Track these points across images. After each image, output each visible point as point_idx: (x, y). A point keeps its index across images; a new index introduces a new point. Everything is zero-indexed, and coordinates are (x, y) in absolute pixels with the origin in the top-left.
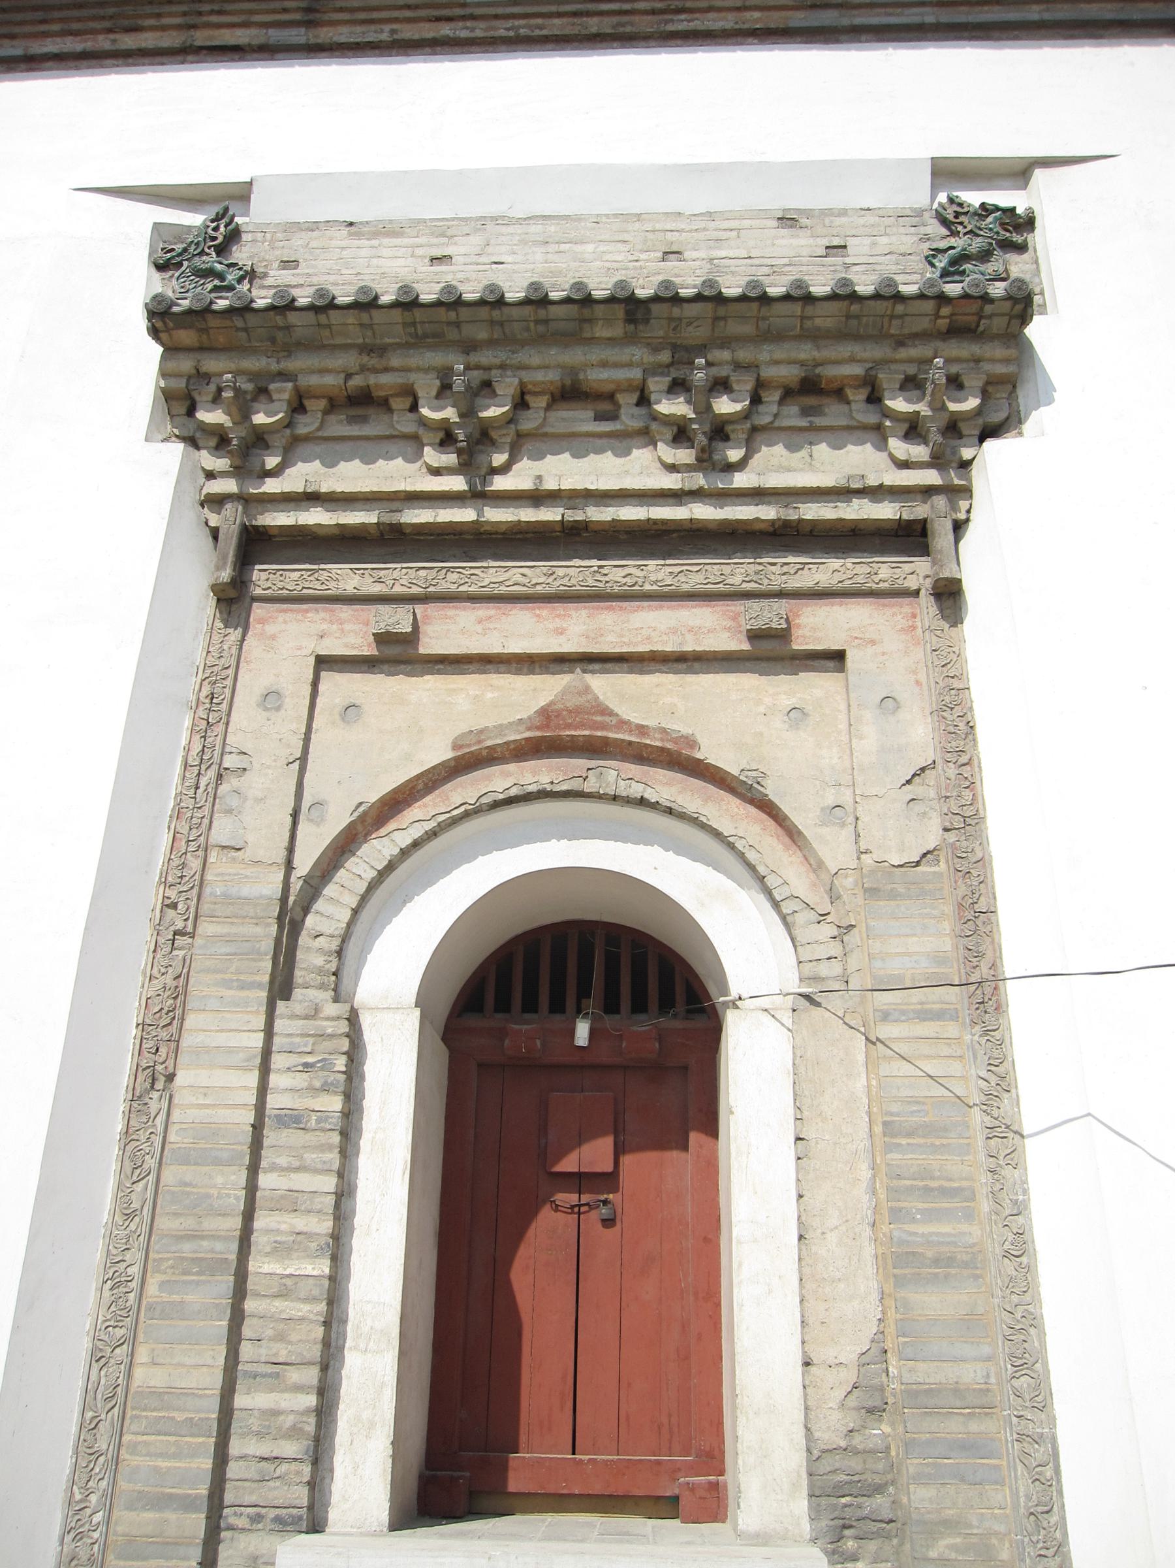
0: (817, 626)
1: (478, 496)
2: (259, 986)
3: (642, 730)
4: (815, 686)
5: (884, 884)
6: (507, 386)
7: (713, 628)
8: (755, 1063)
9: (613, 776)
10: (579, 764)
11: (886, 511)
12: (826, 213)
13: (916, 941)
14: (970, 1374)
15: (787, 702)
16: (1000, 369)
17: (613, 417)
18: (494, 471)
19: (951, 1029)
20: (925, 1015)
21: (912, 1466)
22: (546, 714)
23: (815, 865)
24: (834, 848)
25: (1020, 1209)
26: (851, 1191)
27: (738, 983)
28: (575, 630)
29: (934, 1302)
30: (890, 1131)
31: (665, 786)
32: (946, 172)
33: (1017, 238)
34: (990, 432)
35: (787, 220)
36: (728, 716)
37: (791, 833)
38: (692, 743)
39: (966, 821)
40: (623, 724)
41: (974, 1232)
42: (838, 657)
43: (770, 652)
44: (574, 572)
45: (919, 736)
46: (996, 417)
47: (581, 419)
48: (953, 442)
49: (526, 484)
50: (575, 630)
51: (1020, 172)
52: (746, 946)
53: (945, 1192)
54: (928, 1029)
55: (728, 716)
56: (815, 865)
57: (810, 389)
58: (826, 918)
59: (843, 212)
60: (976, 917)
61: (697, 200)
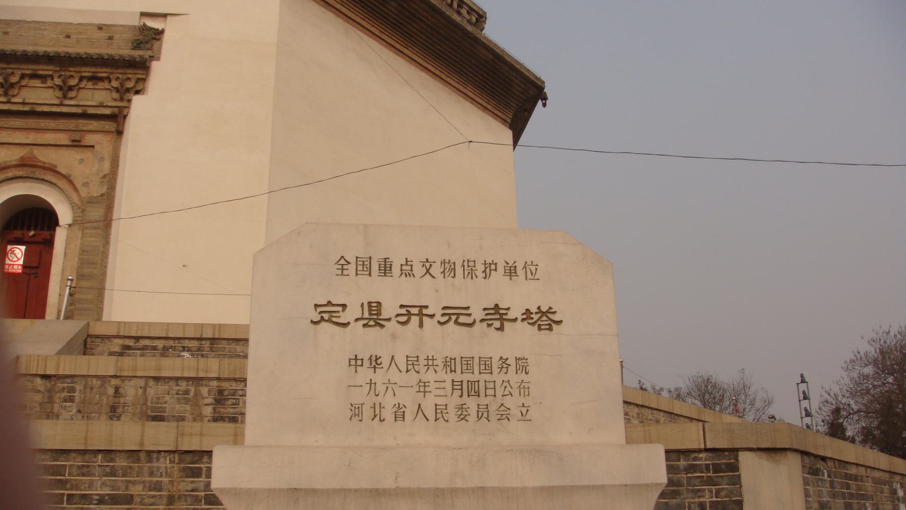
0: (90, 139)
1: (9, 102)
2: (214, 334)
3: (44, 163)
4: (87, 155)
5: (91, 201)
6: (19, 73)
7: (63, 138)
8: (61, 236)
9: (39, 173)
10: (30, 169)
11: (107, 111)
12: (110, 25)
13: (96, 213)
14: (90, 297)
15: (79, 157)
16: (141, 76)
17: (45, 83)
18: (13, 96)
19: (99, 231)
20: (95, 228)
21: (76, 313)
22: (22, 158)
23: (79, 195)
24: (84, 192)
25: (106, 267)
26: (74, 261)
27: (61, 223)
28: (31, 138)
29: (84, 284)
30: (83, 251)
31: (49, 177)
32: (143, 14)
33: (157, 37)
34: (137, 92)
35: (100, 28)
36: (66, 160)
37: (76, 189)
38: (56, 167)
39: (112, 187)
40: (40, 161)
41: (96, 271)
42: (93, 147)
43: (76, 144)
44: (31, 122)
45: (107, 166)
46: (138, 88)
47: (37, 83)
48: (125, 93)
49: (20, 101)
50: (31, 138)
51: (165, 16)
52: (64, 214)
53: (92, 264)
54: (94, 231)
55: (66, 160)
56: (79, 195)
57: (94, 79)
58: (80, 209)
59: (115, 26)
60: (110, 208)
61: (76, 20)
